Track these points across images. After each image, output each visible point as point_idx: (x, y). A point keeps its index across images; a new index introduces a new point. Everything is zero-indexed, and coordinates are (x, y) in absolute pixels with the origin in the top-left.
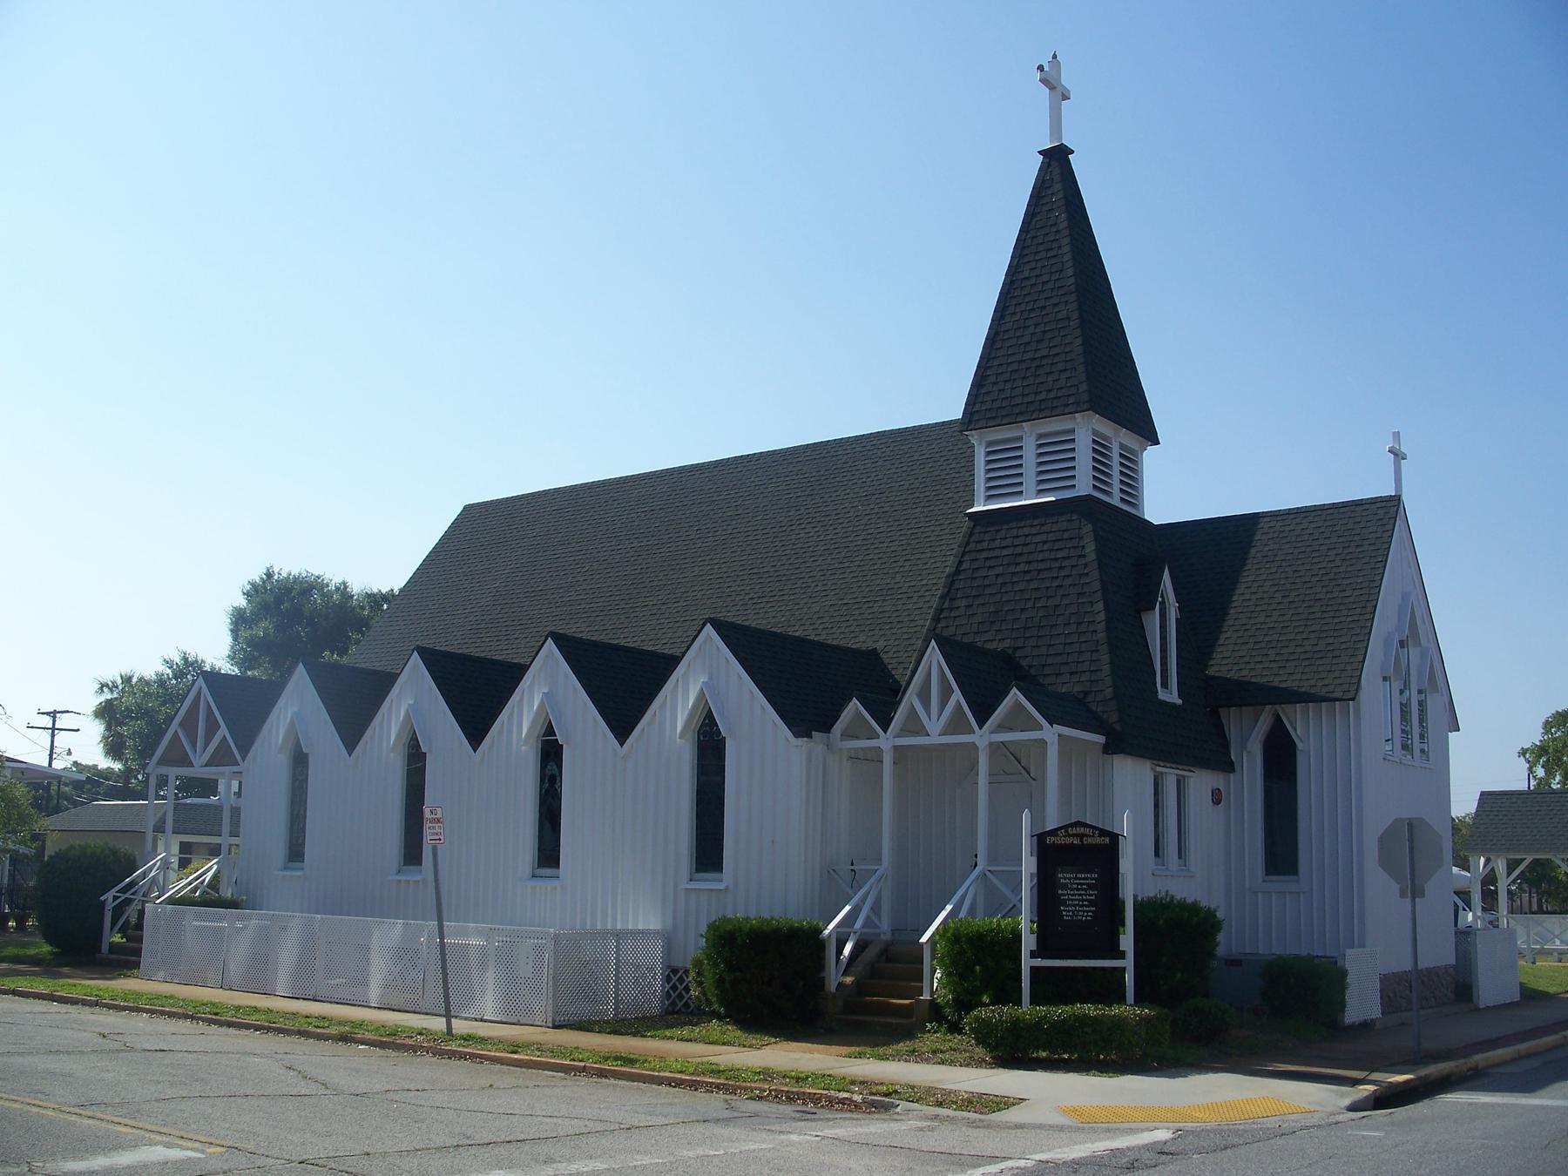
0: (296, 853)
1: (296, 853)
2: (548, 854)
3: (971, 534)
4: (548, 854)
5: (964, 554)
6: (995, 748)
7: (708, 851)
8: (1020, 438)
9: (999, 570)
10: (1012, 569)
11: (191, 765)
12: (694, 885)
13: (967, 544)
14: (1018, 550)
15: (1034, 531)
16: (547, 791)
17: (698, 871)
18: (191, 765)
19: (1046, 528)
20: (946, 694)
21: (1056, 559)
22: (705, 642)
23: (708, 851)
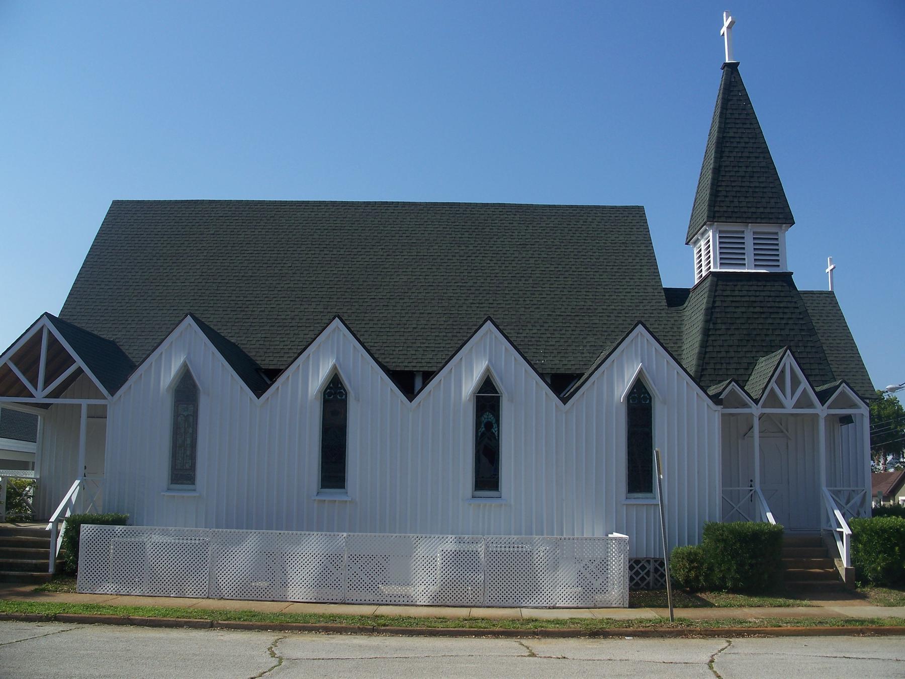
0: (183, 471)
1: (183, 471)
2: (487, 477)
3: (717, 285)
4: (487, 477)
5: (715, 296)
6: (830, 417)
7: (640, 476)
8: (743, 232)
9: (743, 310)
10: (751, 309)
11: (783, 407)
12: (318, 498)
13: (716, 291)
14: (753, 299)
15: (759, 289)
16: (483, 434)
17: (323, 486)
18: (783, 407)
19: (769, 288)
20: (795, 383)
21: (780, 307)
22: (485, 334)
23: (640, 476)
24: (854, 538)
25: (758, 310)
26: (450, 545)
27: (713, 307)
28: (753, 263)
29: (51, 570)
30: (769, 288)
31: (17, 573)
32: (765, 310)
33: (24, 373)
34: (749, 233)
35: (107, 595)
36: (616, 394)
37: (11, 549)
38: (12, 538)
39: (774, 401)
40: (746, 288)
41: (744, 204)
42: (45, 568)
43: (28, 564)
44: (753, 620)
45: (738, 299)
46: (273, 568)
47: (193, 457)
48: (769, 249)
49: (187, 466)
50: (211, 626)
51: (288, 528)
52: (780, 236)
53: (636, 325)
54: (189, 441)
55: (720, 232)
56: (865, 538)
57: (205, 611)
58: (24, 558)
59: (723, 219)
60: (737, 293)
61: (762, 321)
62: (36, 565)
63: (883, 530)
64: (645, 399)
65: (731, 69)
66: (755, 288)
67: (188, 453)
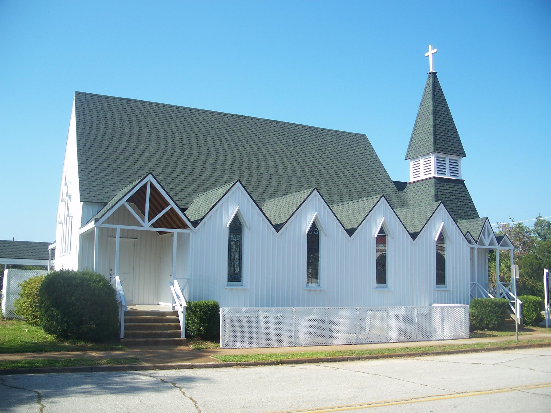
24: (522, 305)
25: (454, 197)
26: (402, 311)
27: (437, 194)
28: (449, 174)
29: (183, 336)
30: (456, 187)
31: (164, 339)
32: (457, 197)
33: (163, 209)
34: (448, 159)
35: (240, 350)
36: (303, 228)
37: (146, 324)
38: (134, 317)
39: (482, 243)
40: (448, 186)
41: (446, 145)
42: (179, 335)
43: (165, 333)
44: (231, 358)
45: (446, 191)
46: (324, 329)
47: (240, 266)
48: (455, 168)
49: (237, 271)
50: (359, 359)
51: (308, 306)
52: (459, 162)
53: (148, 175)
54: (237, 256)
55: (437, 157)
56: (526, 305)
57: (439, 346)
58: (155, 329)
59: (440, 151)
60: (445, 188)
61: (456, 202)
62: (170, 333)
63: (534, 301)
64: (316, 231)
65: (434, 74)
66: (451, 186)
67: (237, 263)
